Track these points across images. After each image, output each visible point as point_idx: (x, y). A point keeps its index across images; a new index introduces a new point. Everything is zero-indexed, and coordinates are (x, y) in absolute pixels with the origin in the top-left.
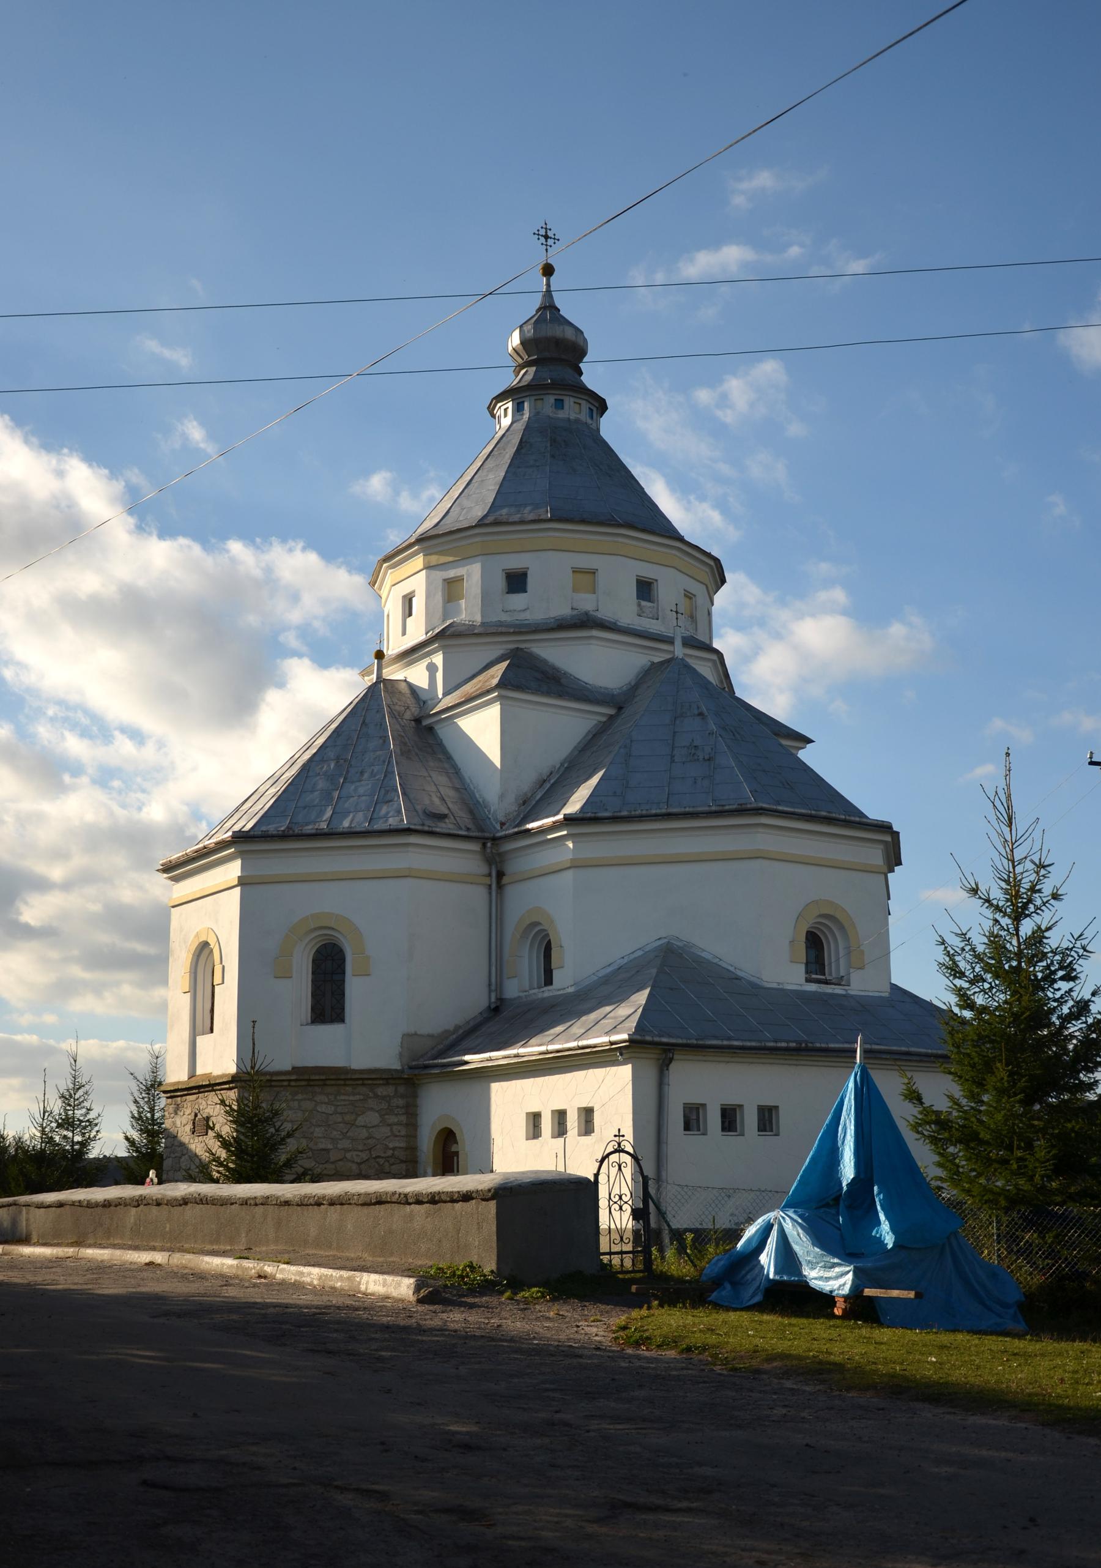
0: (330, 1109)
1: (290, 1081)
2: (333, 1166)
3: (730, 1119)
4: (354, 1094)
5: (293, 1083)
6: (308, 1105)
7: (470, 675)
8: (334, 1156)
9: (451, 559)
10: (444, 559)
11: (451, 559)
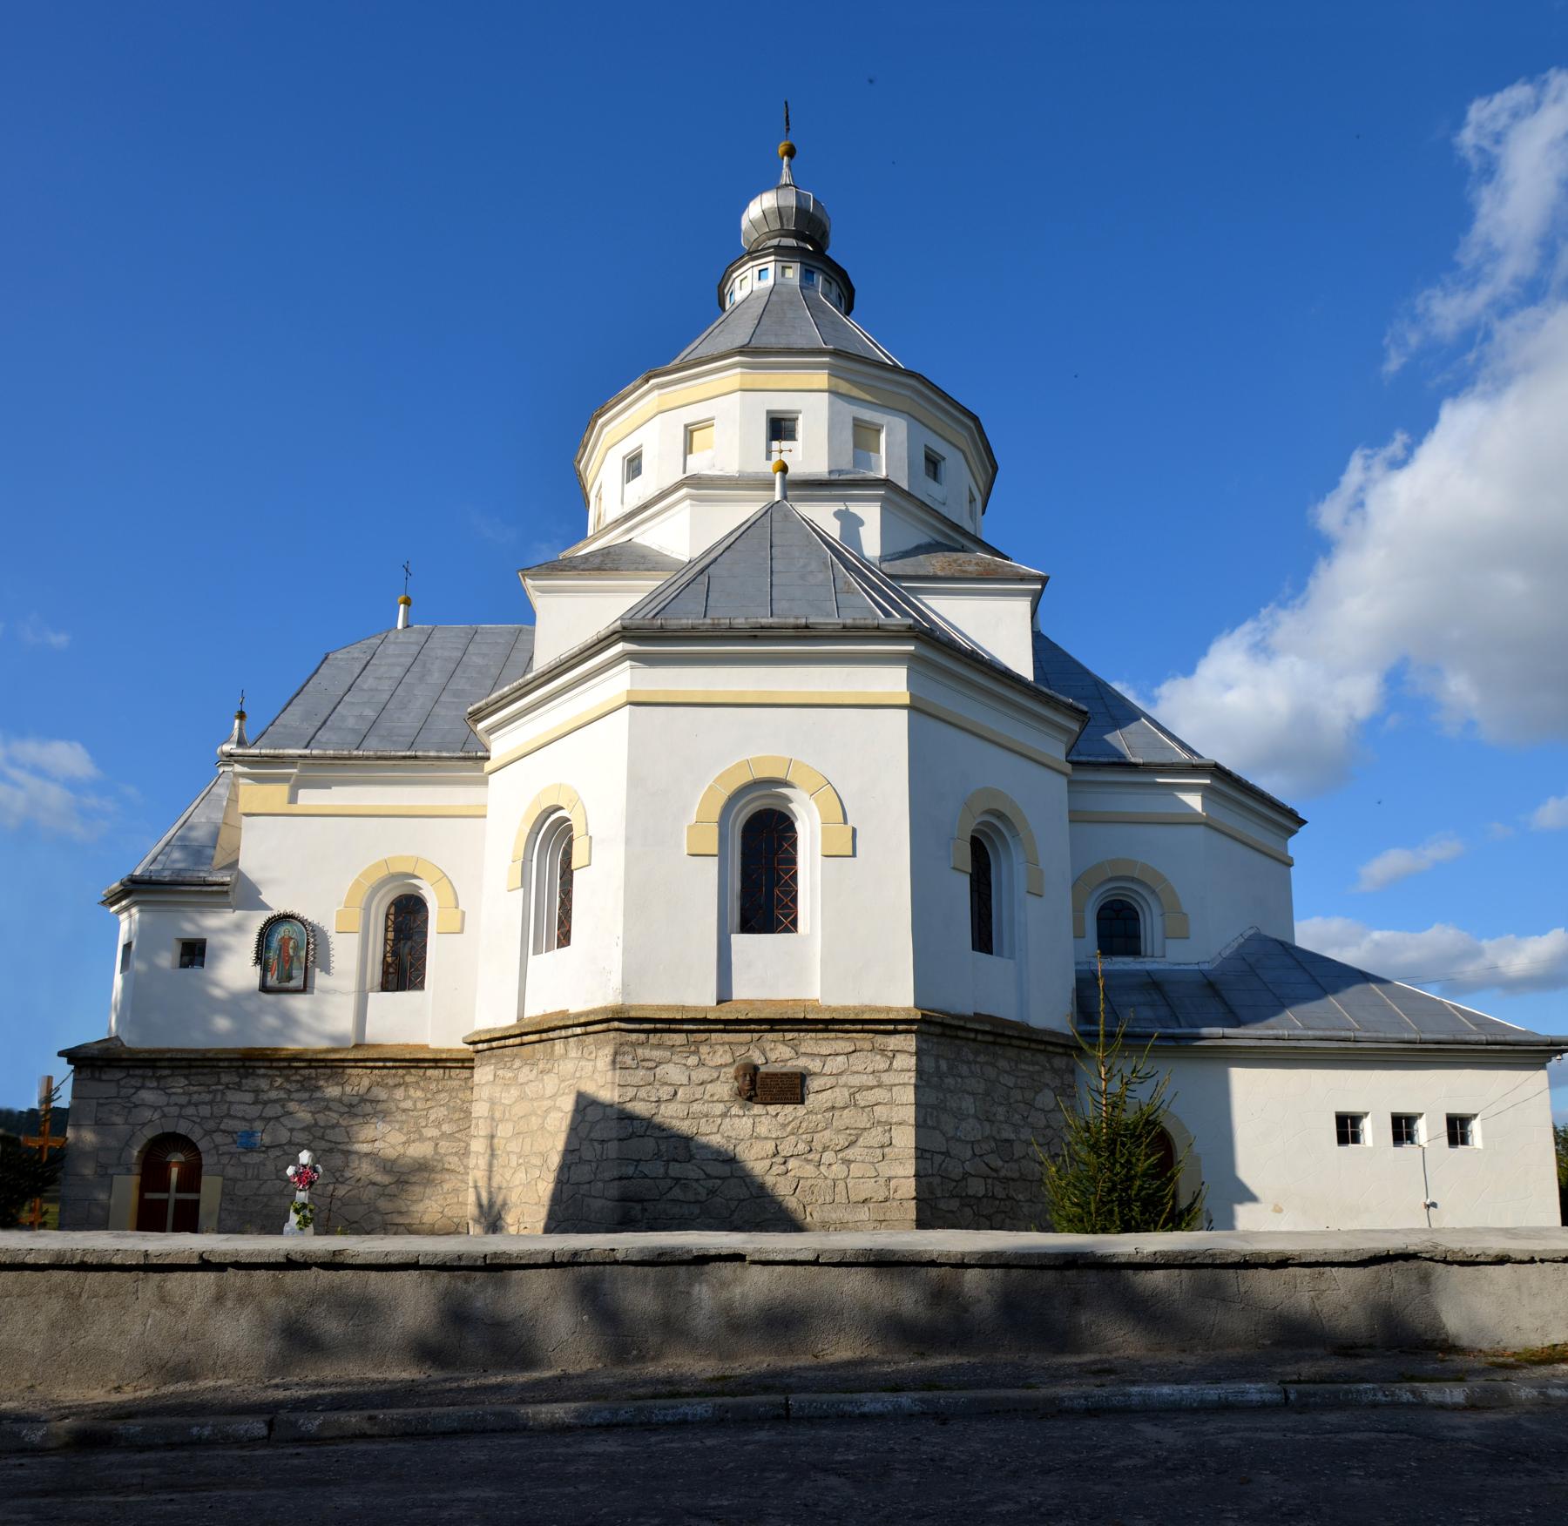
0: (1010, 1081)
1: (977, 1031)
2: (1016, 1166)
3: (1402, 1128)
4: (1034, 1063)
5: (980, 1037)
6: (991, 1072)
7: (286, 701)
8: (1019, 1150)
9: (868, 398)
10: (856, 392)
11: (868, 398)
